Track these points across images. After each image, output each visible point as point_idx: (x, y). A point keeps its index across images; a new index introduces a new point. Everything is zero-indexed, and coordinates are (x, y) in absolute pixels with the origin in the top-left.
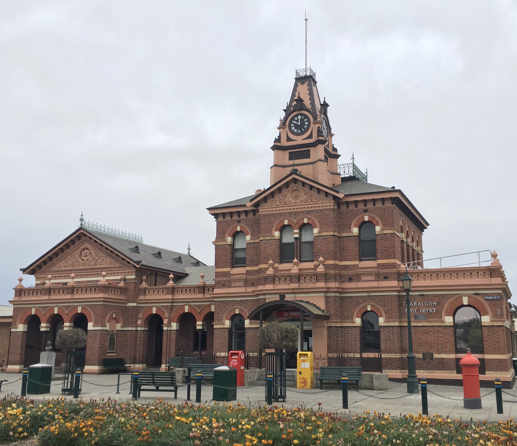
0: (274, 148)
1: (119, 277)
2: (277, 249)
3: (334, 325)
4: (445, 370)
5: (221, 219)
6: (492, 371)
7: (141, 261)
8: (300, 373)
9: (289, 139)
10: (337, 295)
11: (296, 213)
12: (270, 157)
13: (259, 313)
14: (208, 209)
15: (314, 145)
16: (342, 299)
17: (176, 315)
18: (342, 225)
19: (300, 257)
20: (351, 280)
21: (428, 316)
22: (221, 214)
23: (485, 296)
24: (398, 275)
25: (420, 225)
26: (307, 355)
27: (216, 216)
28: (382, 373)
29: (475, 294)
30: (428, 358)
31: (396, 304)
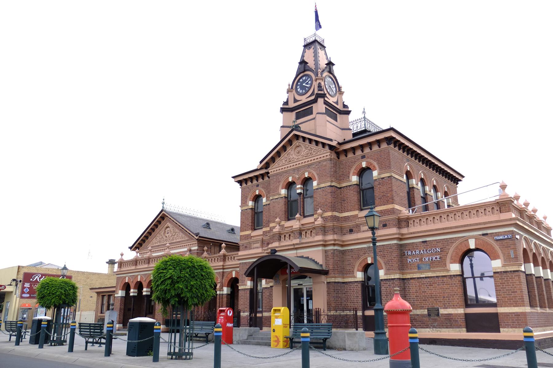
0: (283, 110)
1: (186, 249)
2: (284, 207)
3: (333, 280)
4: (453, 328)
5: (244, 185)
6: (508, 327)
7: (199, 233)
8: (274, 331)
9: (295, 101)
10: (336, 248)
11: (298, 169)
12: (279, 119)
13: (253, 269)
14: (233, 177)
15: (315, 101)
16: (343, 252)
17: (226, 280)
18: (339, 174)
19: (304, 212)
20: (351, 231)
21: (432, 265)
22: (243, 180)
23: (494, 236)
24: (399, 222)
25: (454, 178)
26: (279, 310)
27: (240, 182)
28: (357, 330)
29: (483, 235)
30: (433, 313)
31: (395, 254)
